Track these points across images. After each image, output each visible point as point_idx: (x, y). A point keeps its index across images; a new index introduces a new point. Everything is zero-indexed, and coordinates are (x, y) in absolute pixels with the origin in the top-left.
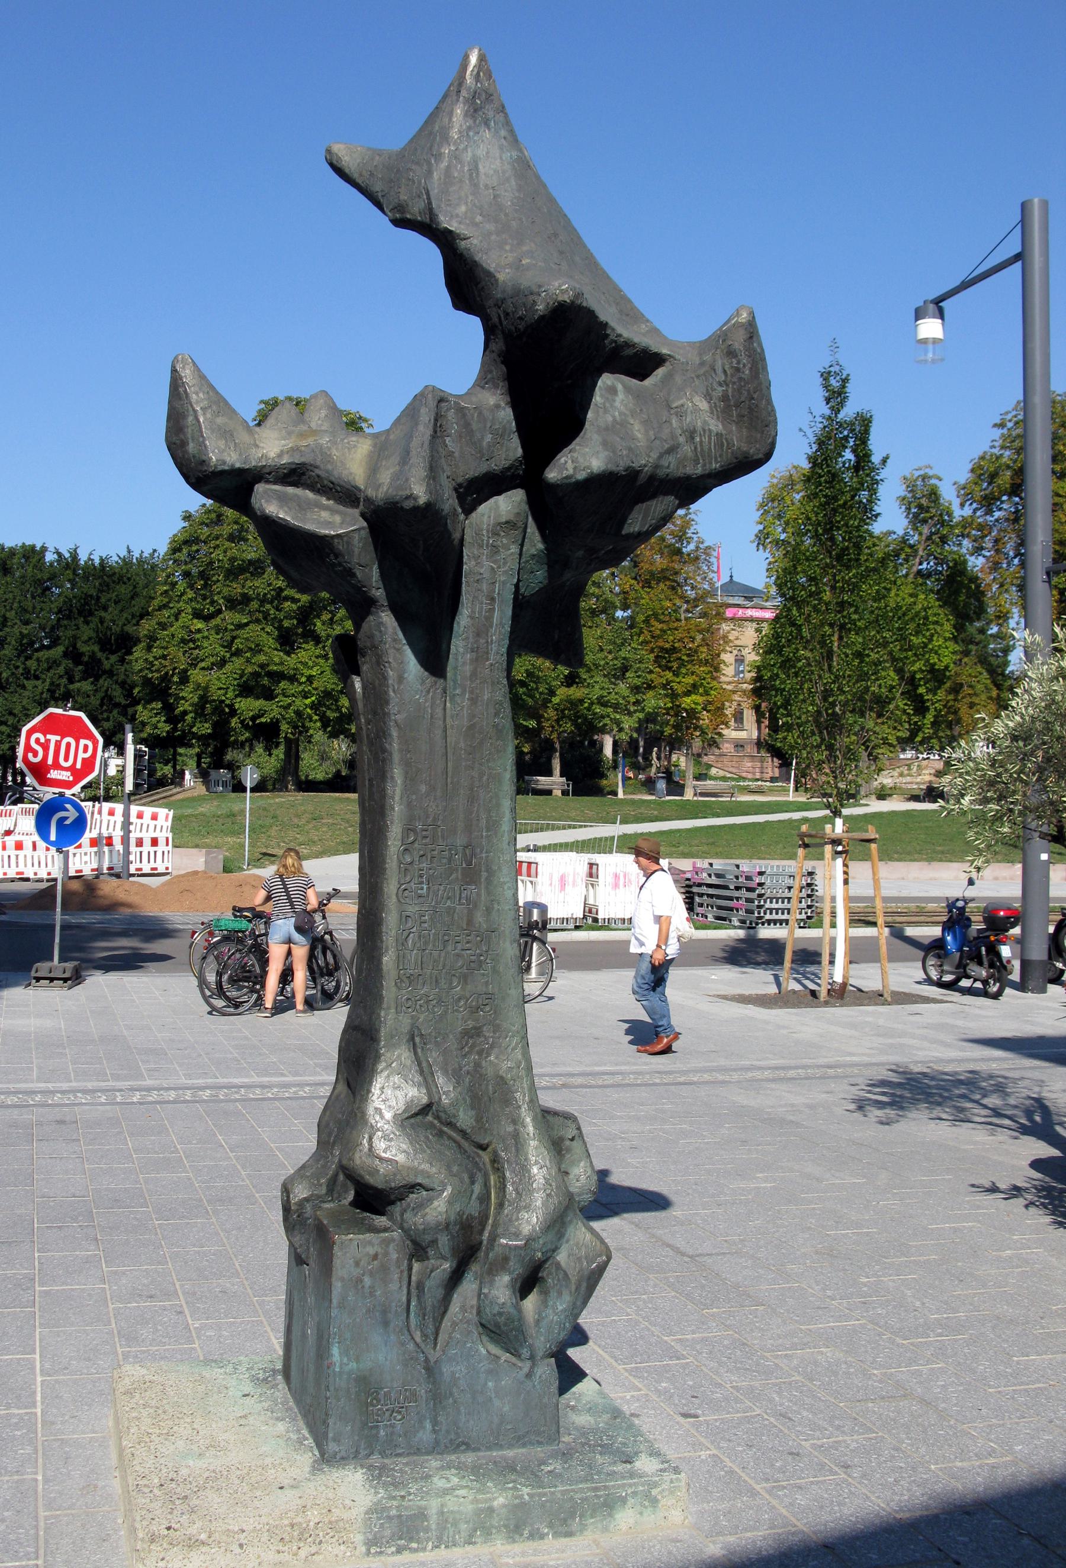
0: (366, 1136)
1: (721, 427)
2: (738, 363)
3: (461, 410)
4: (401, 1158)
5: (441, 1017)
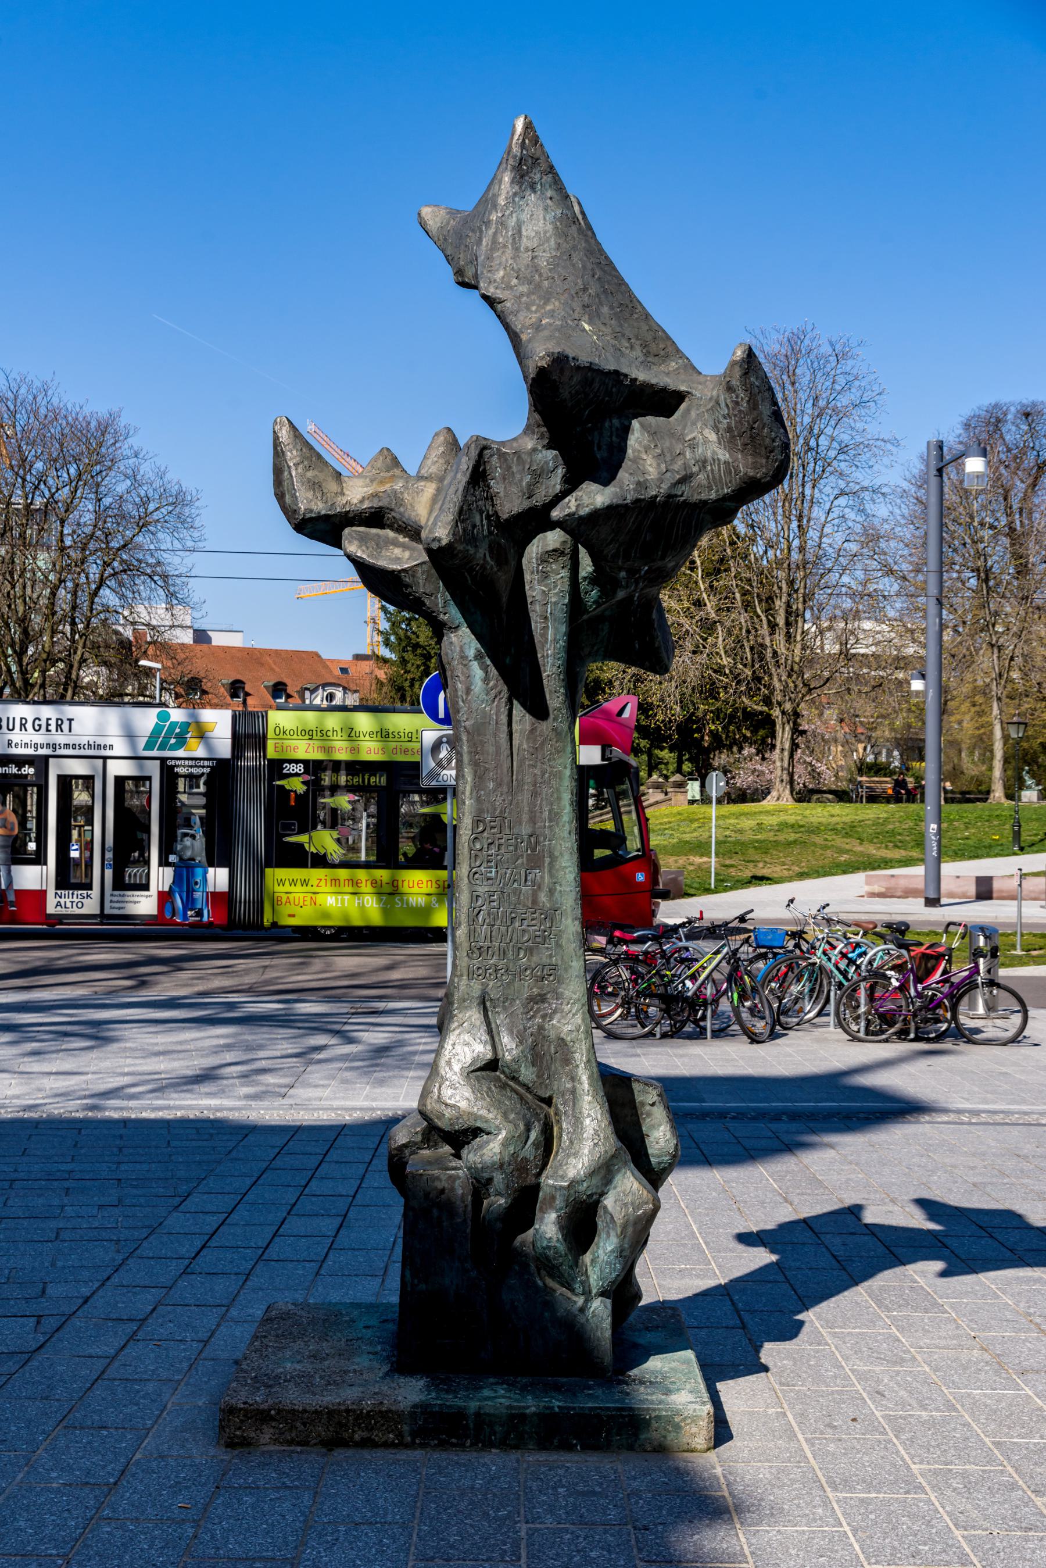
0: (437, 1085)
1: (728, 455)
2: (737, 397)
3: (502, 456)
4: (463, 1105)
5: (509, 984)
